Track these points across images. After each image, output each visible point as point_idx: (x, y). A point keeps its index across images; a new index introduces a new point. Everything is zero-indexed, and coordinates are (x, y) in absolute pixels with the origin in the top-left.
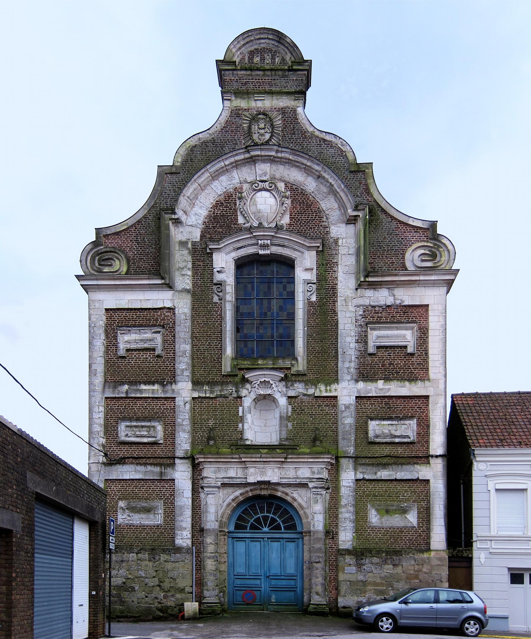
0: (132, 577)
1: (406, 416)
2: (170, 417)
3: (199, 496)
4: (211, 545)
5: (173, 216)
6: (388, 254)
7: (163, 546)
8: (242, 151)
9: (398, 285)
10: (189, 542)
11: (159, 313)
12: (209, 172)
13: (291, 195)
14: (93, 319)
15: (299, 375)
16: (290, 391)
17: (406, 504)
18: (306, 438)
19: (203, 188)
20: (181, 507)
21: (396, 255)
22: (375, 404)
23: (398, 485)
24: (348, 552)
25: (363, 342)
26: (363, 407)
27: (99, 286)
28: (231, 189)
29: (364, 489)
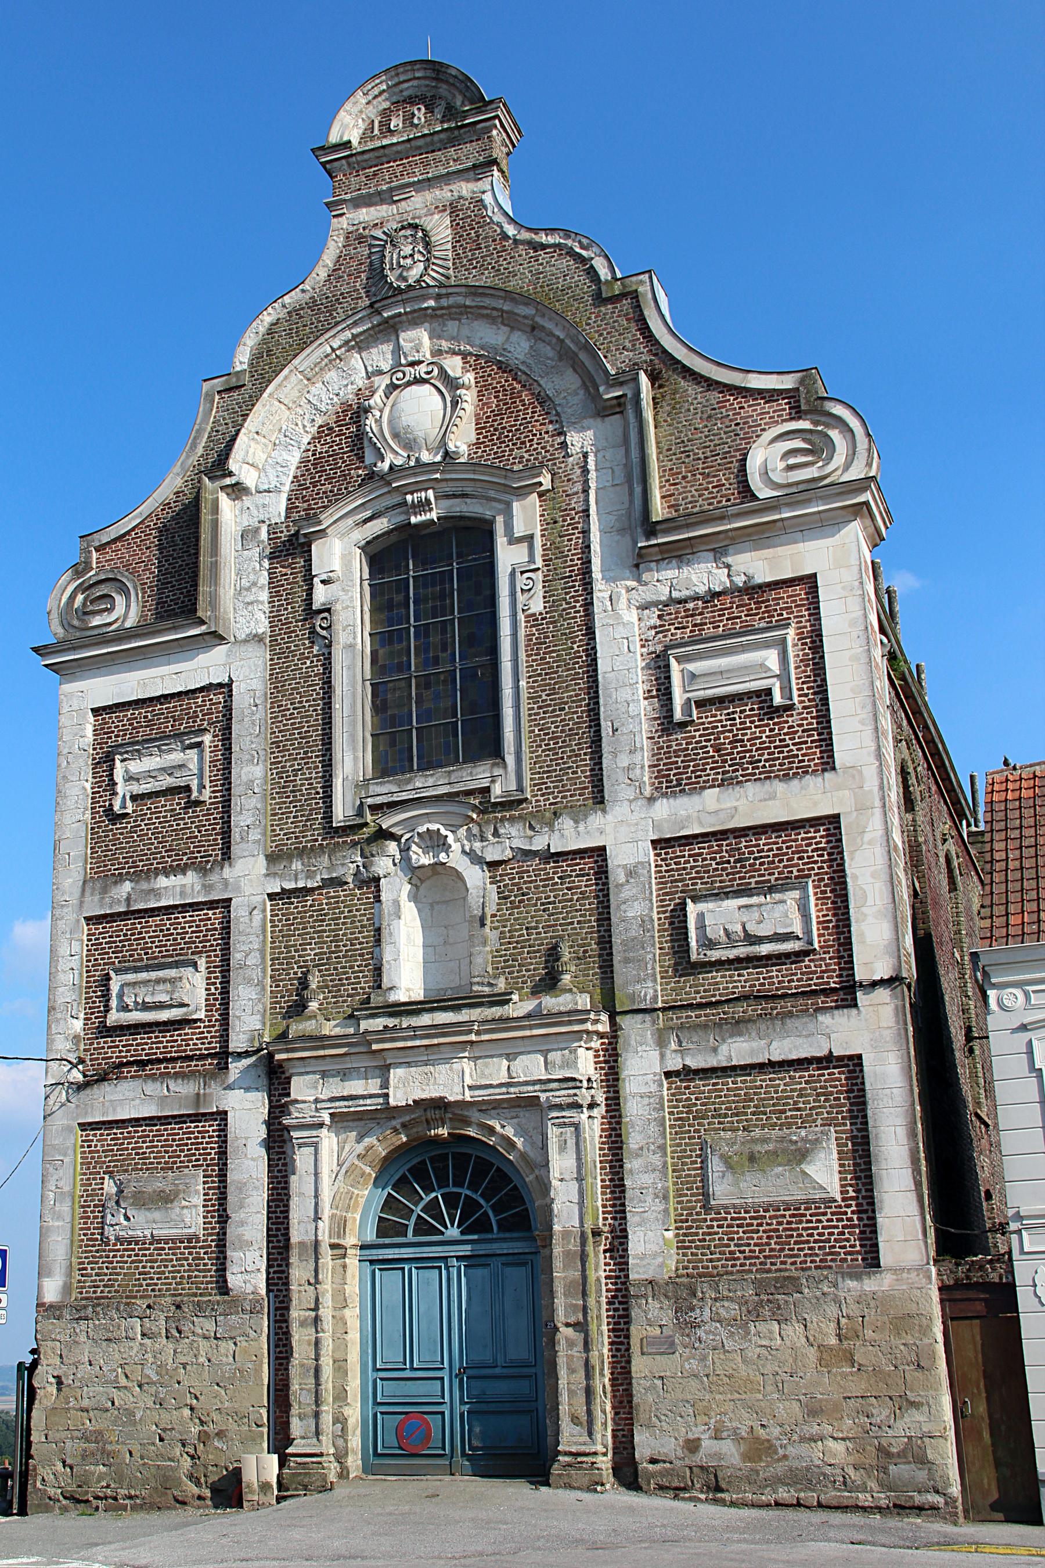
1: (787, 878)
3: (284, 1153)
5: (228, 481)
6: (707, 467)
11: (200, 700)
18: (534, 970)
20: (241, 1187)
26: (674, 866)
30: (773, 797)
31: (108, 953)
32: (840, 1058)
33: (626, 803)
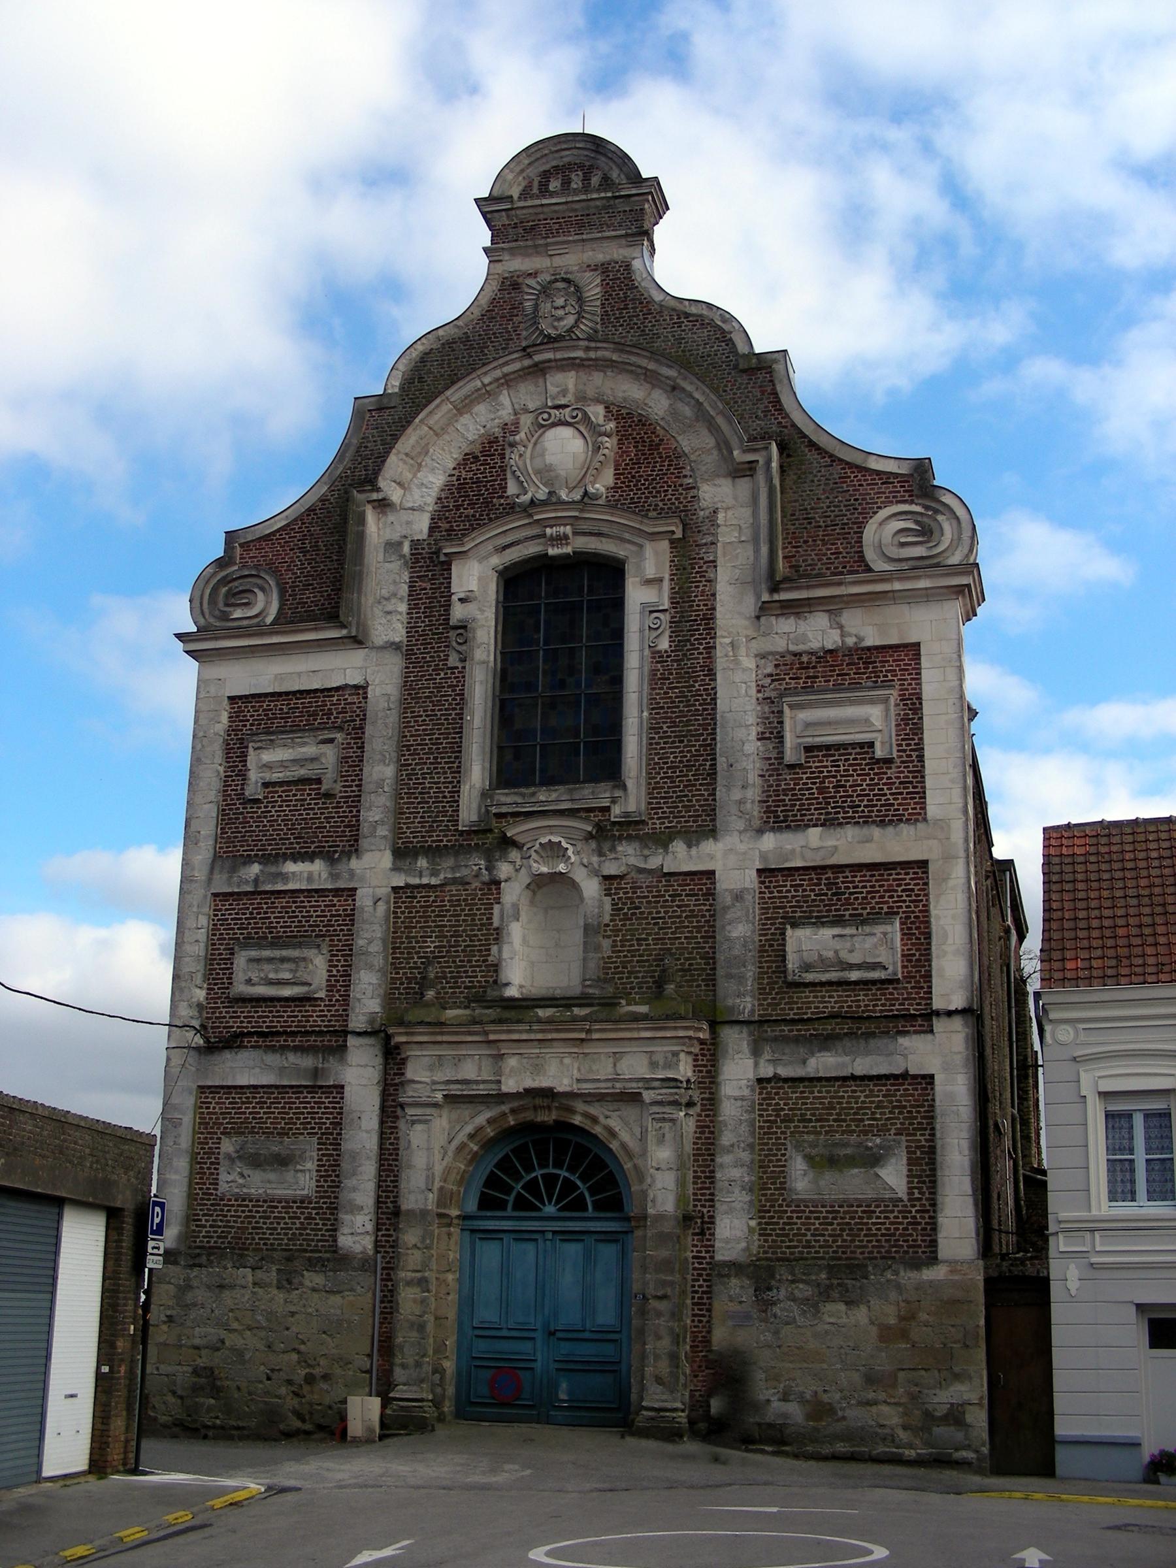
0: (240, 1328)
2: (344, 935)
4: (416, 1252)
5: (375, 496)
7: (312, 1251)
9: (848, 603)
10: (367, 1243)
11: (335, 699)
12: (451, 402)
13: (617, 427)
14: (202, 722)
15: (629, 823)
16: (607, 864)
19: (439, 431)
20: (354, 1156)
22: (803, 885)
23: (861, 1092)
24: (735, 1268)
25: (775, 738)
26: (776, 894)
27: (221, 651)
29: (778, 1104)
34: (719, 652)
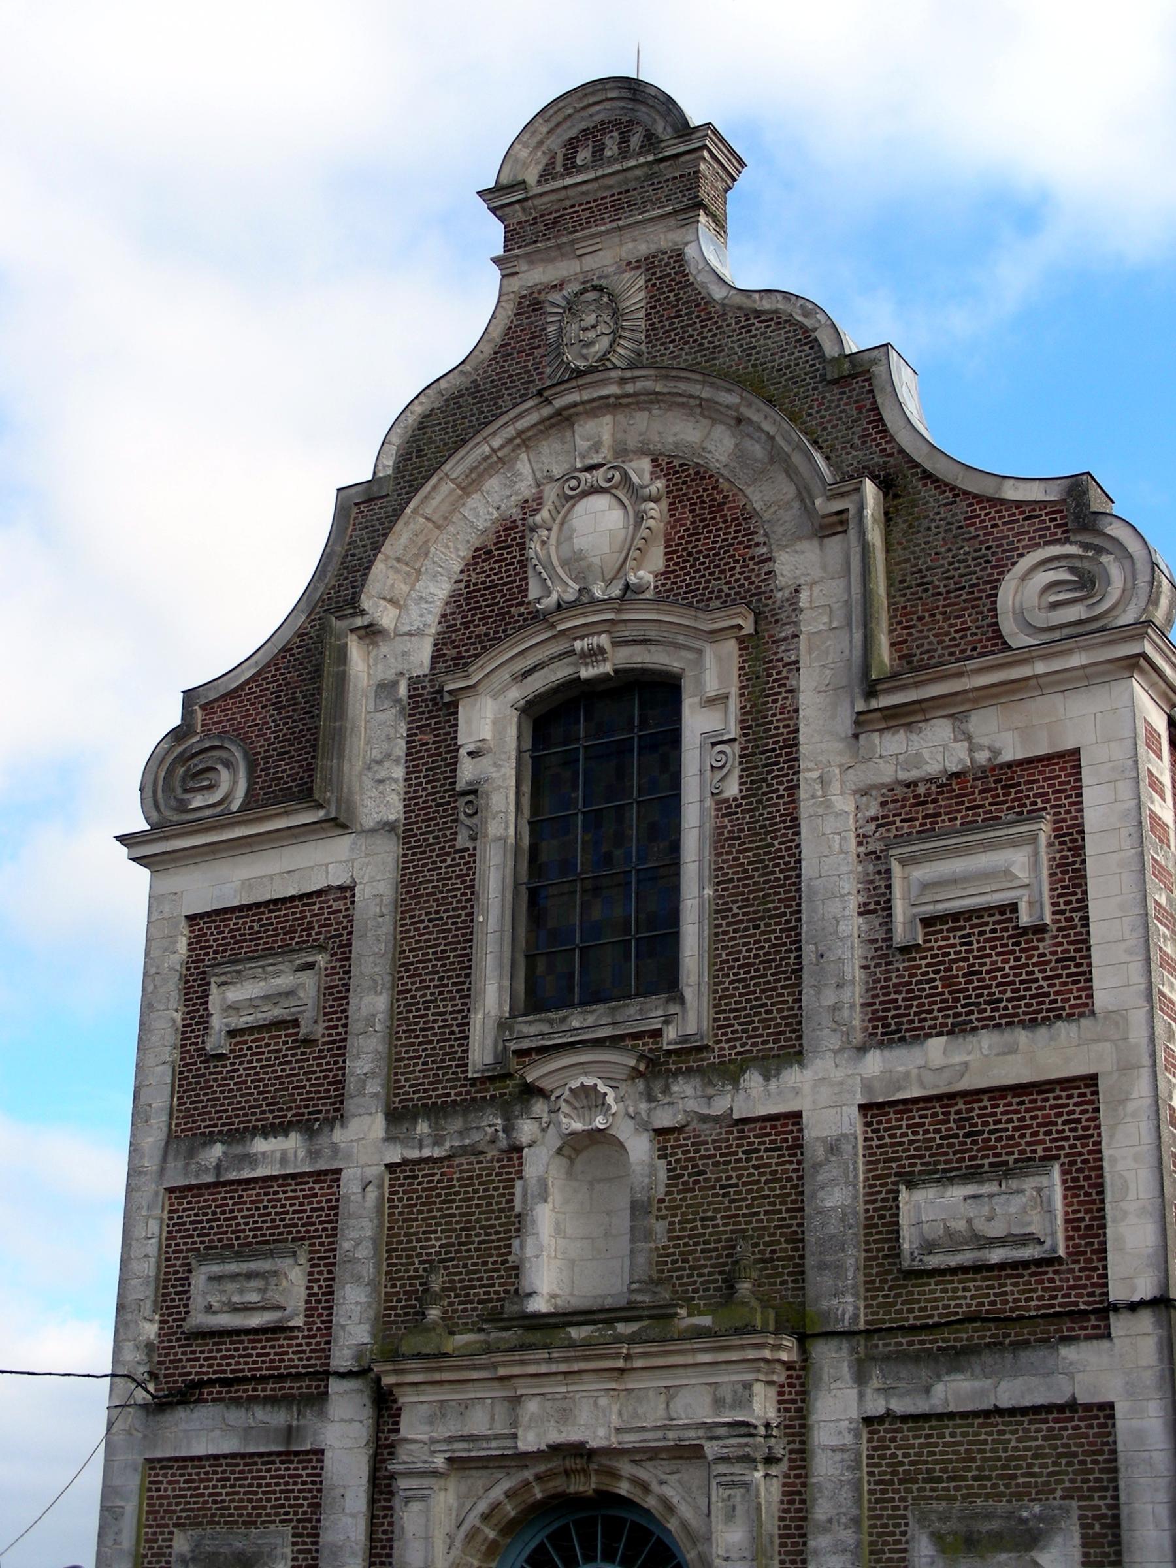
5: (359, 622)
8: (530, 404)
9: (976, 700)
12: (452, 480)
13: (668, 486)
16: (659, 1112)
17: (1037, 1509)
20: (336, 1551)
21: (974, 602)
22: (923, 1124)
28: (511, 507)
29: (894, 1455)
30: (1012, 1050)
31: (192, 1236)
32: (1088, 1407)
33: (830, 1054)
34: (803, 794)
